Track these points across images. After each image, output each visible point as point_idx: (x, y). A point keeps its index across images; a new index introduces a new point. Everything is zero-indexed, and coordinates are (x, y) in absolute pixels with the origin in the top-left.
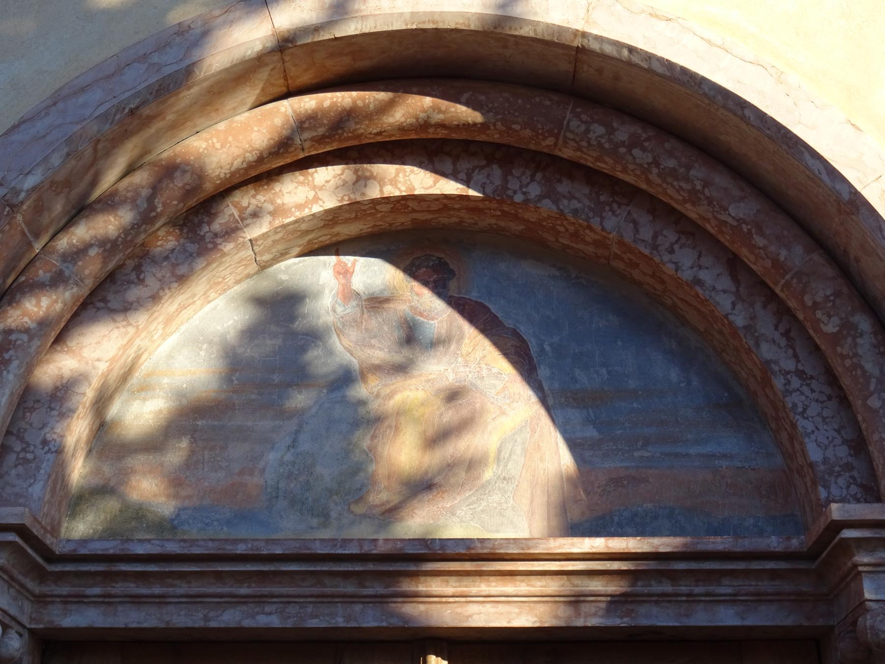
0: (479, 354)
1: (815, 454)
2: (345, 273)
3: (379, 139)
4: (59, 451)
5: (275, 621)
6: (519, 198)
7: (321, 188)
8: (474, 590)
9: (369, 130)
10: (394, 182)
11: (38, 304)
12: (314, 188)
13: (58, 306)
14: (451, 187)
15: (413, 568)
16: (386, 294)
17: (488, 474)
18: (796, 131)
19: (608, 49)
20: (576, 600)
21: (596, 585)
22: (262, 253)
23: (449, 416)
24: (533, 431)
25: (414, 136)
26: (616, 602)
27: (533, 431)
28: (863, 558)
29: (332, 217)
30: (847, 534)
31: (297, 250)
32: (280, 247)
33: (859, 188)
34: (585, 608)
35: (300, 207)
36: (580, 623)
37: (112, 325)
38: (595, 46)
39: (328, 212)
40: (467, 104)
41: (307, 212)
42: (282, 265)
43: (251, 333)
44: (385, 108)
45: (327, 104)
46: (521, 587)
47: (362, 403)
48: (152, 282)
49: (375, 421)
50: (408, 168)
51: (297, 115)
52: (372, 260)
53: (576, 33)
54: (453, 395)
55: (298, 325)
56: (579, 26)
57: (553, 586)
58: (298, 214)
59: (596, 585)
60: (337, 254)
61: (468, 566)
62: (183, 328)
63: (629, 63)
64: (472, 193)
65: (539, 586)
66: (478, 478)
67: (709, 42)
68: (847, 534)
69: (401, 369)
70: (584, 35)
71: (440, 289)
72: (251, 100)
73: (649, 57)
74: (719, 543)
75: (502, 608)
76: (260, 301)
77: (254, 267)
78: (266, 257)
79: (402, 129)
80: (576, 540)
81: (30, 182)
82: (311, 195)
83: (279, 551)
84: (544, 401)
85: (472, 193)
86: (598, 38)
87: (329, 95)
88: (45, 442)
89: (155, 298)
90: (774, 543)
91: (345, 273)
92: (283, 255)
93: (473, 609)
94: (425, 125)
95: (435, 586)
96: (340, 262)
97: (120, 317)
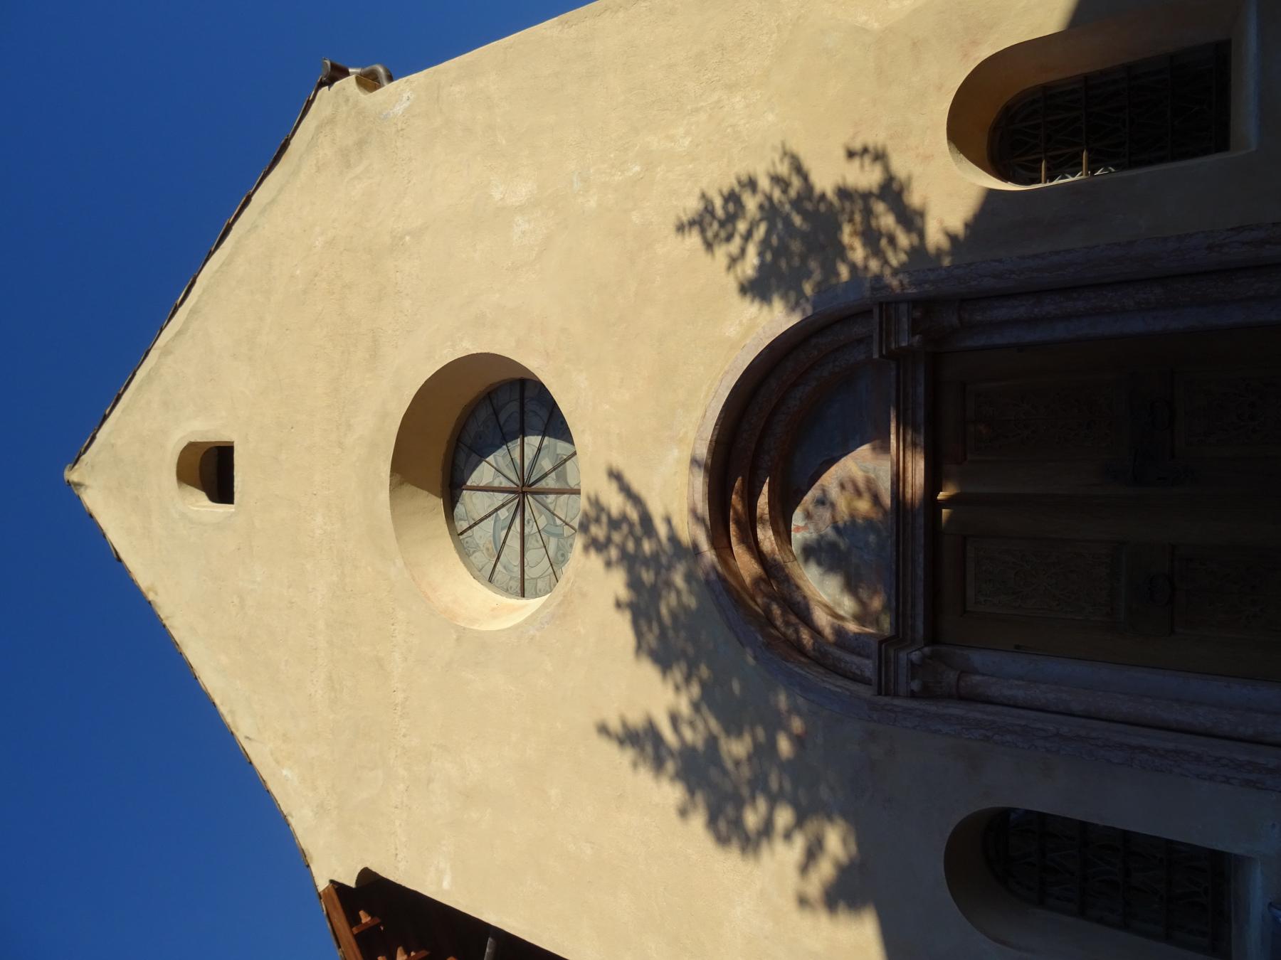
0: (829, 479)
1: (862, 357)
2: (798, 529)
3: (747, 514)
4: (859, 634)
5: (921, 556)
6: (769, 464)
7: (765, 536)
8: (910, 482)
9: (744, 518)
10: (763, 510)
11: (805, 639)
12: (765, 539)
13: (806, 632)
14: (765, 488)
15: (901, 504)
16: (806, 513)
17: (873, 476)
18: (745, 367)
19: (716, 433)
20: (914, 445)
21: (909, 438)
22: (789, 559)
23: (849, 486)
24: (857, 459)
25: (747, 501)
26: (915, 430)
27: (857, 459)
28: (893, 346)
29: (776, 532)
30: (884, 352)
31: (789, 546)
32: (787, 552)
33: (765, 346)
34: (917, 441)
35: (772, 544)
36: (923, 443)
37: (814, 614)
38: (715, 437)
39: (774, 535)
40: (735, 482)
41: (774, 542)
42: (795, 552)
43: (819, 563)
44: (736, 512)
45: (734, 533)
46: (909, 465)
47: (845, 524)
48: (799, 599)
49: (853, 516)
50: (758, 504)
51: (739, 544)
52: (793, 518)
53: (710, 444)
54: (842, 486)
55: (816, 547)
56: (708, 442)
57: (909, 454)
58: (775, 545)
59: (909, 438)
60: (791, 531)
61: (901, 484)
62: (818, 590)
63: (721, 425)
64: (767, 481)
65: (909, 458)
66: (874, 479)
67: (713, 398)
68: (884, 352)
69: (833, 505)
70: (711, 441)
71: (805, 493)
72: (733, 561)
73: (719, 418)
74: (893, 394)
75: (917, 472)
76: (806, 560)
77: (795, 562)
78: (791, 557)
79: (744, 506)
80: (891, 448)
81: (760, 638)
82: (767, 540)
83: (895, 553)
84: (846, 454)
85: (767, 481)
86: (712, 436)
87: (731, 533)
88: (856, 639)
89: (805, 597)
90: (893, 373)
91: (798, 529)
92: (791, 552)
93: (917, 482)
94: (742, 498)
95: (909, 496)
96: (794, 531)
97: (811, 611)
